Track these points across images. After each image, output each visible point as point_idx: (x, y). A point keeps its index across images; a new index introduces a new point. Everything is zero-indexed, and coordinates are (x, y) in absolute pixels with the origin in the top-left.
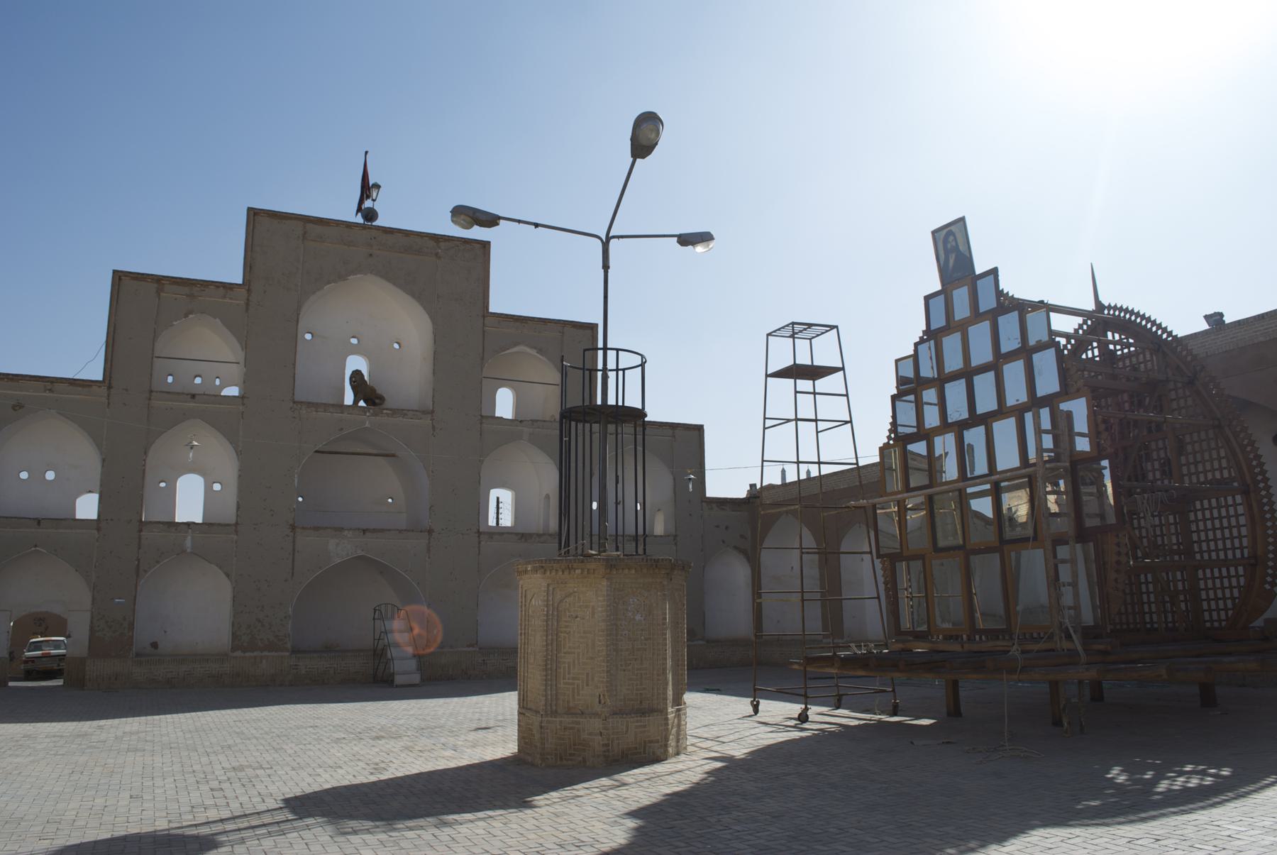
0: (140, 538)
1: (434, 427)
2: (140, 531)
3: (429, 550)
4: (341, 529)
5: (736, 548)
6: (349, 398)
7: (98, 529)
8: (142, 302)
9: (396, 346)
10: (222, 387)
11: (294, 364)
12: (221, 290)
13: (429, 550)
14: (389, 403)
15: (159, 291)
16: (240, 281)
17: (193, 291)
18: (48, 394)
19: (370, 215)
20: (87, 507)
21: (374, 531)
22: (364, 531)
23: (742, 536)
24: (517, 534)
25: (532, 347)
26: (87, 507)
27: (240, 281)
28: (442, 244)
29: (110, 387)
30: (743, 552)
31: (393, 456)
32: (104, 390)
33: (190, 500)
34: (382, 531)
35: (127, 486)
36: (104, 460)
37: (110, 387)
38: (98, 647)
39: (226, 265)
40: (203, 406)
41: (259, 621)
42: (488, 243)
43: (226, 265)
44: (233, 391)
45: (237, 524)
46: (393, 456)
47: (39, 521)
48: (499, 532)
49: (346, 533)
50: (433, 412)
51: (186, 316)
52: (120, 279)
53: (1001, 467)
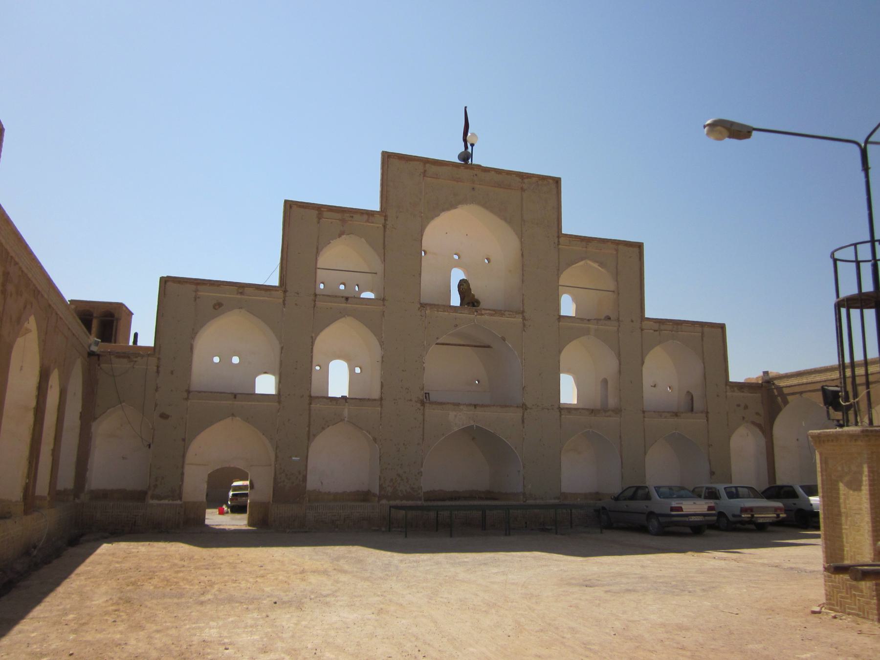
0: (310, 410)
1: (524, 325)
2: (310, 404)
3: (523, 422)
4: (458, 404)
5: (753, 423)
6: (455, 300)
7: (279, 402)
8: (307, 225)
9: (456, 257)
10: (361, 292)
11: (420, 274)
12: (365, 217)
13: (523, 422)
14: (483, 305)
15: (320, 217)
16: (378, 209)
17: (343, 219)
18: (239, 296)
19: (466, 157)
20: (266, 384)
21: (483, 406)
22: (475, 406)
23: (757, 414)
24: (587, 409)
25: (595, 261)
26: (266, 384)
27: (378, 209)
28: (526, 181)
29: (285, 291)
30: (759, 426)
31: (489, 347)
32: (280, 293)
33: (338, 381)
34: (444, 404)
35: (297, 372)
36: (282, 348)
37: (285, 291)
38: (280, 494)
39: (366, 196)
40: (347, 305)
41: (399, 475)
42: (560, 179)
43: (366, 196)
44: (368, 295)
45: (381, 399)
46: (489, 347)
47: (235, 396)
48: (569, 409)
49: (461, 407)
50: (523, 312)
51: (340, 236)
52: (291, 207)
53: (869, 357)
